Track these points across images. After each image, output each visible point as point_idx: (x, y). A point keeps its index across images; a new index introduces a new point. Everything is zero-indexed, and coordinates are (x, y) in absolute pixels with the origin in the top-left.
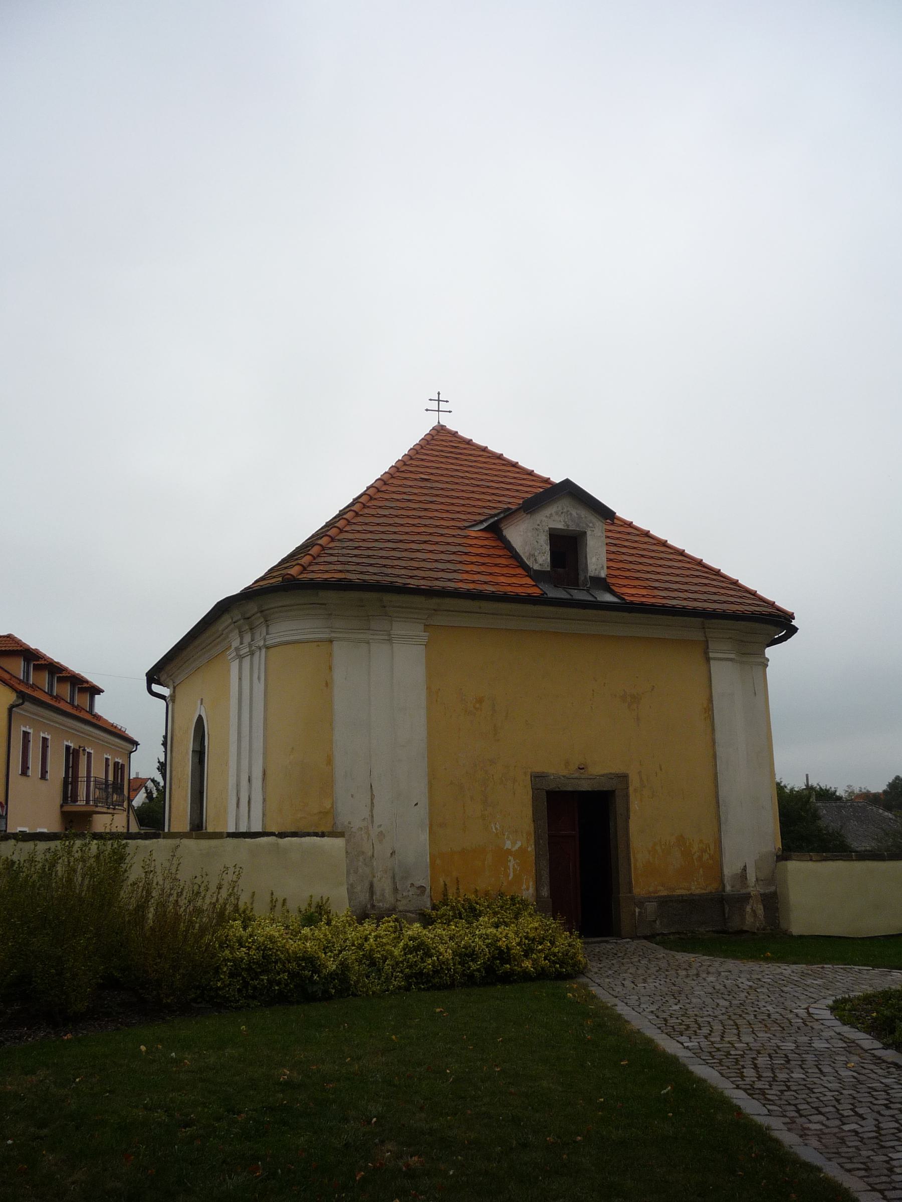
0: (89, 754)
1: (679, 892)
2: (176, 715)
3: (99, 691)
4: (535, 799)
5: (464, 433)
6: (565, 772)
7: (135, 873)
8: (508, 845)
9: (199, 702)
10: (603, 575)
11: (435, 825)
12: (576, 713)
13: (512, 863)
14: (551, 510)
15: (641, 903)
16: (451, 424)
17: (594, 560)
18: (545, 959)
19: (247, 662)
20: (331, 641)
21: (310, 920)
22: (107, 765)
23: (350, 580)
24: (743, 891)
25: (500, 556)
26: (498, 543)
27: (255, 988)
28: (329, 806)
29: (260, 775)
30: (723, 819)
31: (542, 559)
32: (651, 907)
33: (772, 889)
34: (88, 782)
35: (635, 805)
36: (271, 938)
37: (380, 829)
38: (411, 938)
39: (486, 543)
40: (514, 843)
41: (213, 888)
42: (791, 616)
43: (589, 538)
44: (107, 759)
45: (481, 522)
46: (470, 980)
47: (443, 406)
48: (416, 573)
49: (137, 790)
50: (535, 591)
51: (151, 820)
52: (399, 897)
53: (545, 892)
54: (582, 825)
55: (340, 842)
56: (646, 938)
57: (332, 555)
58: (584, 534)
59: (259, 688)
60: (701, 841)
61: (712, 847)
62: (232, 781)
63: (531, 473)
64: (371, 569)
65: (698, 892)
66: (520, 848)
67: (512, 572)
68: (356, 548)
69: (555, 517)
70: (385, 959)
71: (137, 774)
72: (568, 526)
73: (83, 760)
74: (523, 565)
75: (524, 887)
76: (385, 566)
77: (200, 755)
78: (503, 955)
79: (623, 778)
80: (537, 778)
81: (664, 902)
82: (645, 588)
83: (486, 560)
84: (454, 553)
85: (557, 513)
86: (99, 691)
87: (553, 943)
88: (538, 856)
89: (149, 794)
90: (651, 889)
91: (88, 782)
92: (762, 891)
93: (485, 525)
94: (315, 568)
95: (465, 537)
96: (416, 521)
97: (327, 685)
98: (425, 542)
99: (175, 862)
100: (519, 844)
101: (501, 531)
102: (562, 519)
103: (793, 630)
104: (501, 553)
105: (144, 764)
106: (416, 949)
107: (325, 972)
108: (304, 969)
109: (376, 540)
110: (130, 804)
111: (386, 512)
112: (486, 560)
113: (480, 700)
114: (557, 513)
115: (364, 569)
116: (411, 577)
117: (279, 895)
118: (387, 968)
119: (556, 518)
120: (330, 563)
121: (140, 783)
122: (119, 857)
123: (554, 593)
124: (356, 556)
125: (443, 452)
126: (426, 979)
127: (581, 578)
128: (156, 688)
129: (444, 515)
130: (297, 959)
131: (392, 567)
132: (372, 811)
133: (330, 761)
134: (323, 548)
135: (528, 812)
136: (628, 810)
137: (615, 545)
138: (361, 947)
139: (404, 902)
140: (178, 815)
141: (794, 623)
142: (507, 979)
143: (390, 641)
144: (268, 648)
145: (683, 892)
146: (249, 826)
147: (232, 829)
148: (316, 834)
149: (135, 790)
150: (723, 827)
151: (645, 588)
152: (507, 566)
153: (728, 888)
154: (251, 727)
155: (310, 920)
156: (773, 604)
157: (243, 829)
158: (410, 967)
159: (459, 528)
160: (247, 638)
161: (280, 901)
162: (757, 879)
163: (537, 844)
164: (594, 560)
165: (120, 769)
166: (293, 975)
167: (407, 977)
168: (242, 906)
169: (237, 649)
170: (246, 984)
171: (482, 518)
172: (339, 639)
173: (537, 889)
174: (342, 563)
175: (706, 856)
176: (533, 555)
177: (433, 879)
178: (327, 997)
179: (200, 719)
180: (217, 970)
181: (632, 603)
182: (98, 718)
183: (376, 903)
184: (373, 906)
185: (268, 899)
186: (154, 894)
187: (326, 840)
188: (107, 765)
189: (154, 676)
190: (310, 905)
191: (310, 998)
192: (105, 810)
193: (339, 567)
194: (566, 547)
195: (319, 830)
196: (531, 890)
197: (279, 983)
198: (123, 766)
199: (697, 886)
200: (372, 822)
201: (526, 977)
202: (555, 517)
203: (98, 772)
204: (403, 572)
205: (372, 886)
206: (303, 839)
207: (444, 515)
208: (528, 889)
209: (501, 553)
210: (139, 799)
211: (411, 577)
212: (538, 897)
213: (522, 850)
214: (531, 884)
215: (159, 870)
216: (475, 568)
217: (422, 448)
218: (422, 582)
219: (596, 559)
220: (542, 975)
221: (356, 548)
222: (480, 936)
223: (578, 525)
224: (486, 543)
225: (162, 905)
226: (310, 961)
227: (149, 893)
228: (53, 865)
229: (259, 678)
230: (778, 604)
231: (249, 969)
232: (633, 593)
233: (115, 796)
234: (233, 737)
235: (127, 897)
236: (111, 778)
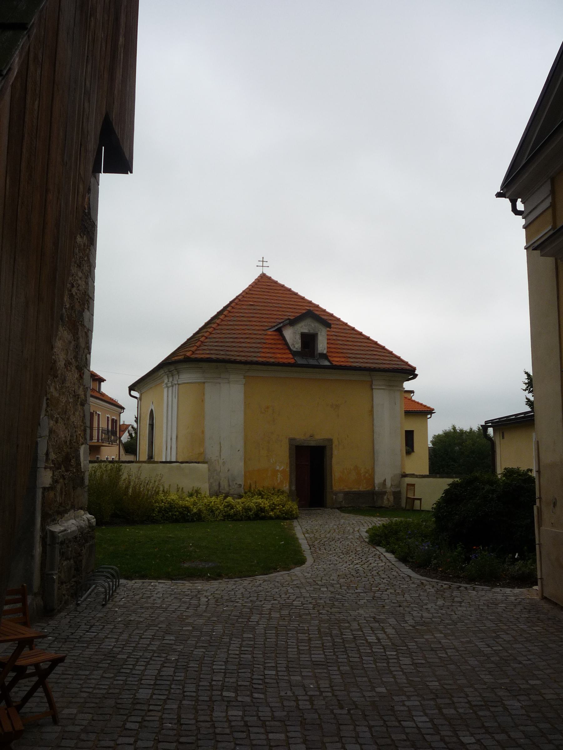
0: (99, 414)
1: (354, 490)
3: (103, 380)
4: (290, 449)
5: (274, 278)
7: (125, 476)
8: (278, 468)
10: (325, 352)
11: (247, 460)
12: (309, 412)
14: (302, 324)
15: (336, 494)
17: (321, 346)
18: (280, 512)
19: (170, 389)
20: (204, 383)
21: (191, 495)
22: (108, 420)
23: (212, 358)
24: (384, 490)
25: (280, 344)
26: (280, 337)
27: (167, 517)
29: (175, 437)
32: (341, 496)
33: (398, 489)
34: (98, 430)
35: (335, 452)
36: (173, 500)
38: (226, 502)
39: (274, 337)
40: (280, 468)
41: (153, 481)
42: (414, 369)
43: (319, 336)
44: (108, 417)
45: (274, 326)
46: (249, 519)
47: (265, 264)
48: (241, 354)
49: (124, 431)
50: (292, 361)
51: (131, 448)
52: (231, 488)
53: (294, 488)
55: (205, 466)
56: (338, 508)
57: (205, 345)
58: (317, 334)
59: (175, 401)
62: (164, 439)
63: (303, 298)
64: (222, 353)
67: (284, 351)
68: (216, 342)
69: (305, 327)
70: (217, 510)
71: (124, 422)
73: (96, 418)
74: (289, 348)
76: (227, 351)
77: (152, 426)
78: (262, 510)
79: (330, 441)
80: (291, 440)
81: (347, 494)
82: (344, 357)
83: (273, 346)
84: (259, 343)
85: (305, 325)
86: (103, 380)
87: (283, 507)
89: (130, 435)
91: (98, 430)
92: (394, 490)
93: (276, 328)
94: (198, 352)
95: (266, 335)
96: (243, 328)
98: (247, 338)
99: (140, 472)
101: (282, 331)
102: (307, 328)
103: (415, 376)
104: (280, 342)
105: (128, 417)
106: (228, 506)
107: (192, 512)
108: (185, 511)
109: (226, 338)
110: (120, 441)
111: (231, 323)
112: (273, 346)
113: (268, 408)
115: (218, 352)
116: (238, 356)
117: (180, 486)
118: (217, 512)
120: (204, 350)
121: (125, 428)
122: (119, 470)
123: (300, 361)
124: (216, 346)
126: (231, 517)
128: (133, 393)
129: (258, 324)
130: (182, 507)
131: (231, 351)
133: (203, 432)
134: (202, 342)
135: (287, 454)
136: (332, 454)
137: (336, 336)
138: (209, 505)
140: (143, 454)
141: (416, 373)
142: (264, 518)
143: (229, 383)
144: (179, 384)
145: (356, 490)
146: (171, 459)
147: (164, 460)
148: (196, 462)
149: (123, 431)
151: (344, 357)
152: (282, 349)
153: (377, 489)
154: (172, 416)
155: (191, 495)
156: (407, 363)
157: (168, 460)
159: (264, 330)
160: (171, 379)
161: (181, 488)
162: (392, 485)
164: (321, 346)
165: (114, 422)
166: (181, 513)
167: (224, 516)
168: (165, 490)
169: (166, 384)
171: (275, 324)
173: (290, 487)
174: (210, 350)
175: (367, 475)
178: (192, 521)
179: (152, 411)
180: (154, 510)
181: (336, 365)
182: (103, 395)
186: (132, 483)
187: (200, 464)
188: (108, 420)
189: (132, 388)
191: (187, 521)
192: (107, 445)
193: (208, 352)
194: (309, 340)
195: (198, 461)
196: (287, 487)
197: (175, 515)
198: (116, 420)
199: (363, 488)
201: (271, 518)
202: (305, 327)
203: (103, 425)
204: (236, 353)
205: (219, 483)
207: (258, 324)
208: (286, 486)
209: (280, 342)
210: (125, 438)
211: (238, 356)
212: (290, 490)
215: (133, 475)
216: (267, 350)
217: (253, 287)
218: (243, 358)
219: (322, 346)
220: (278, 518)
221: (216, 342)
222: (254, 503)
224: (274, 337)
225: (134, 487)
226: (187, 508)
227: (129, 482)
228: (95, 472)
230: (410, 363)
231: (165, 510)
232: (337, 360)
233: (112, 437)
234: (165, 421)
235: (122, 484)
236: (110, 428)
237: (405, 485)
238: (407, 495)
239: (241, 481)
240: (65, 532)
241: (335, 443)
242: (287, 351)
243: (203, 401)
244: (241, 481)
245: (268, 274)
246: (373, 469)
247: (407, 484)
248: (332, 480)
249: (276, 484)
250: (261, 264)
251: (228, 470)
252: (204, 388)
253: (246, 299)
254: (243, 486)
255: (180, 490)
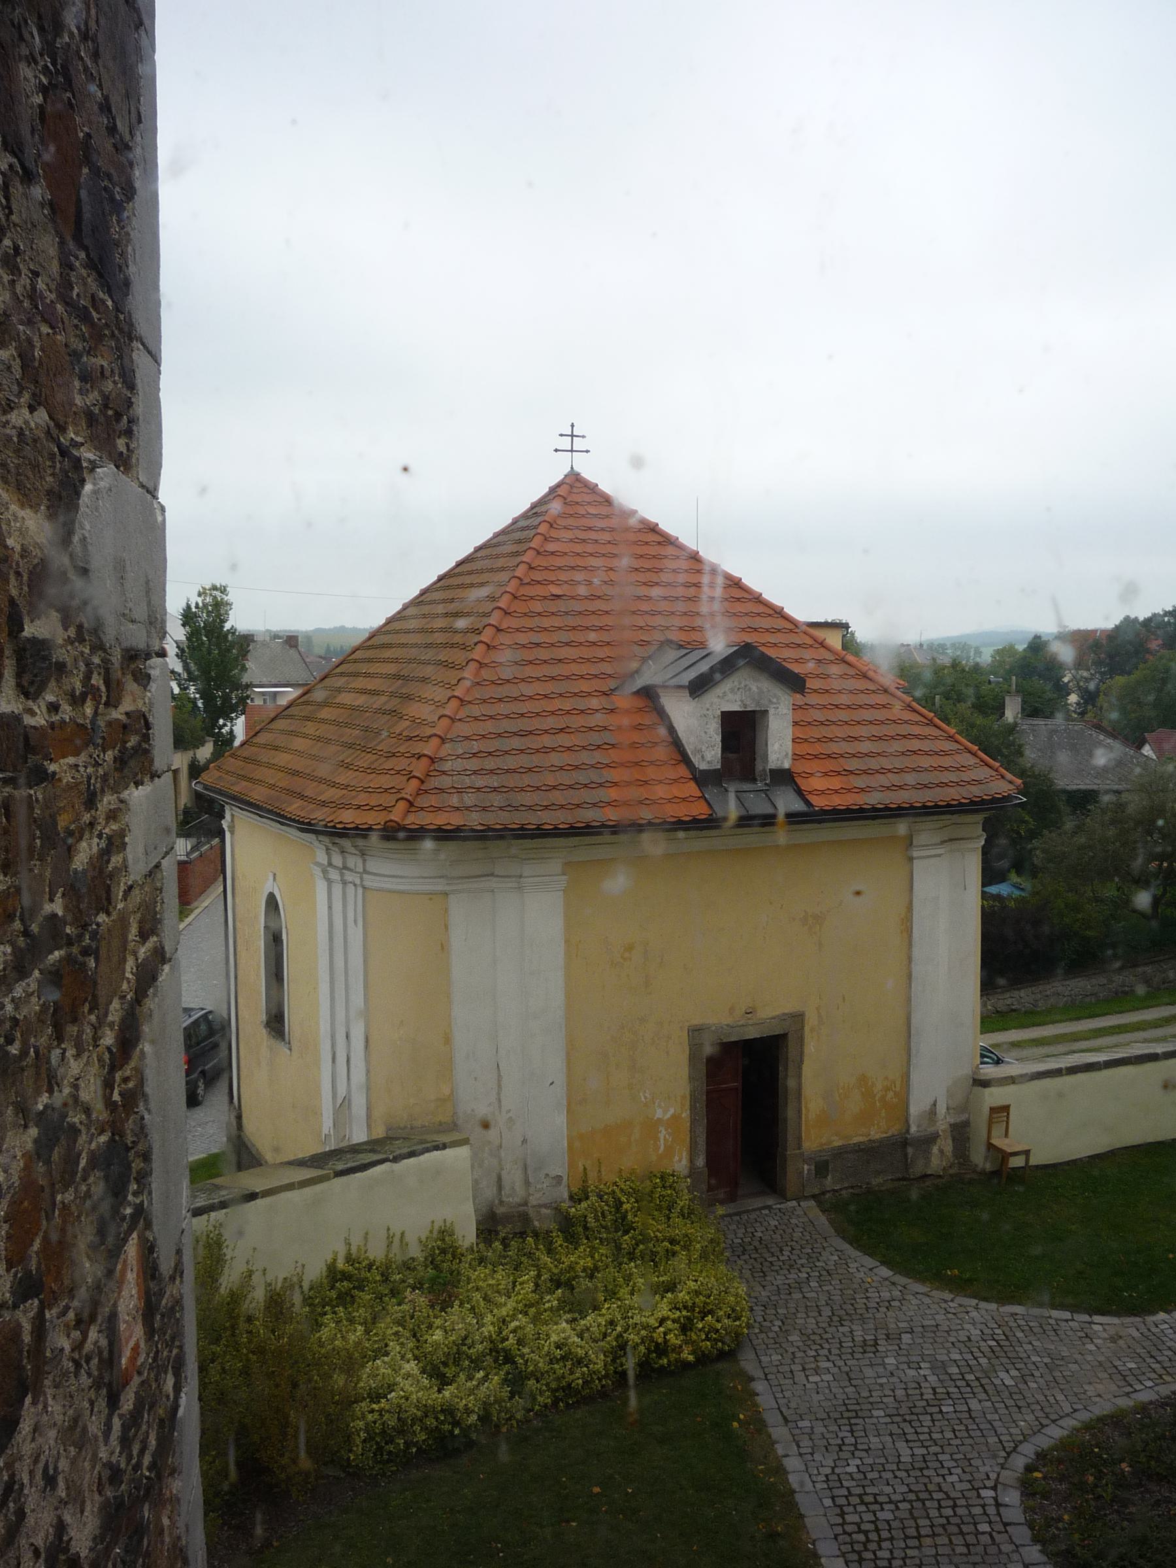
1: (855, 1140)
2: (237, 851)
6: (729, 1021)
8: (659, 1114)
9: (271, 878)
11: (574, 1103)
13: (663, 1133)
14: (726, 686)
16: (589, 474)
17: (776, 746)
24: (932, 1129)
28: (447, 1092)
30: (913, 1051)
31: (707, 750)
33: (964, 1117)
35: (810, 1047)
37: (510, 1115)
43: (771, 718)
47: (578, 444)
53: (701, 1162)
54: (747, 1081)
60: (886, 1078)
61: (898, 1084)
62: (324, 1027)
65: (877, 1137)
66: (673, 1116)
72: (745, 706)
74: (685, 759)
75: (677, 1158)
85: (732, 690)
88: (693, 1122)
90: (824, 1141)
92: (952, 1121)
97: (443, 948)
100: (672, 1111)
102: (737, 697)
108: (442, 1422)
113: (630, 948)
114: (732, 690)
117: (396, 1230)
119: (730, 696)
125: (575, 505)
127: (759, 767)
132: (499, 1094)
133: (448, 1040)
136: (802, 1054)
139: (538, 1195)
143: (520, 888)
145: (861, 1139)
150: (914, 1061)
153: (913, 1129)
158: (558, 1379)
163: (693, 1108)
164: (776, 746)
170: (380, 1448)
172: (453, 892)
173: (691, 1161)
175: (890, 1094)
176: (700, 751)
177: (572, 1165)
183: (504, 1199)
184: (501, 1202)
185: (383, 1234)
190: (431, 1232)
196: (685, 1162)
199: (876, 1132)
200: (500, 1107)
205: (499, 1179)
206: (422, 1158)
208: (680, 1161)
212: (693, 1172)
213: (675, 1117)
214: (684, 1154)
219: (779, 746)
223: (758, 704)
229: (355, 921)
232: (823, 789)
237: (986, 1111)
238: (989, 1137)
239: (559, 1168)
240: (47, 897)
241: (811, 1020)
242: (683, 771)
243: (444, 947)
244: (559, 1168)
245: (588, 475)
246: (906, 1077)
247: (992, 1109)
248: (800, 1124)
249: (654, 1158)
250: (566, 443)
251: (524, 1141)
252: (446, 910)
253: (537, 576)
254: (565, 1178)
255: (396, 1240)
